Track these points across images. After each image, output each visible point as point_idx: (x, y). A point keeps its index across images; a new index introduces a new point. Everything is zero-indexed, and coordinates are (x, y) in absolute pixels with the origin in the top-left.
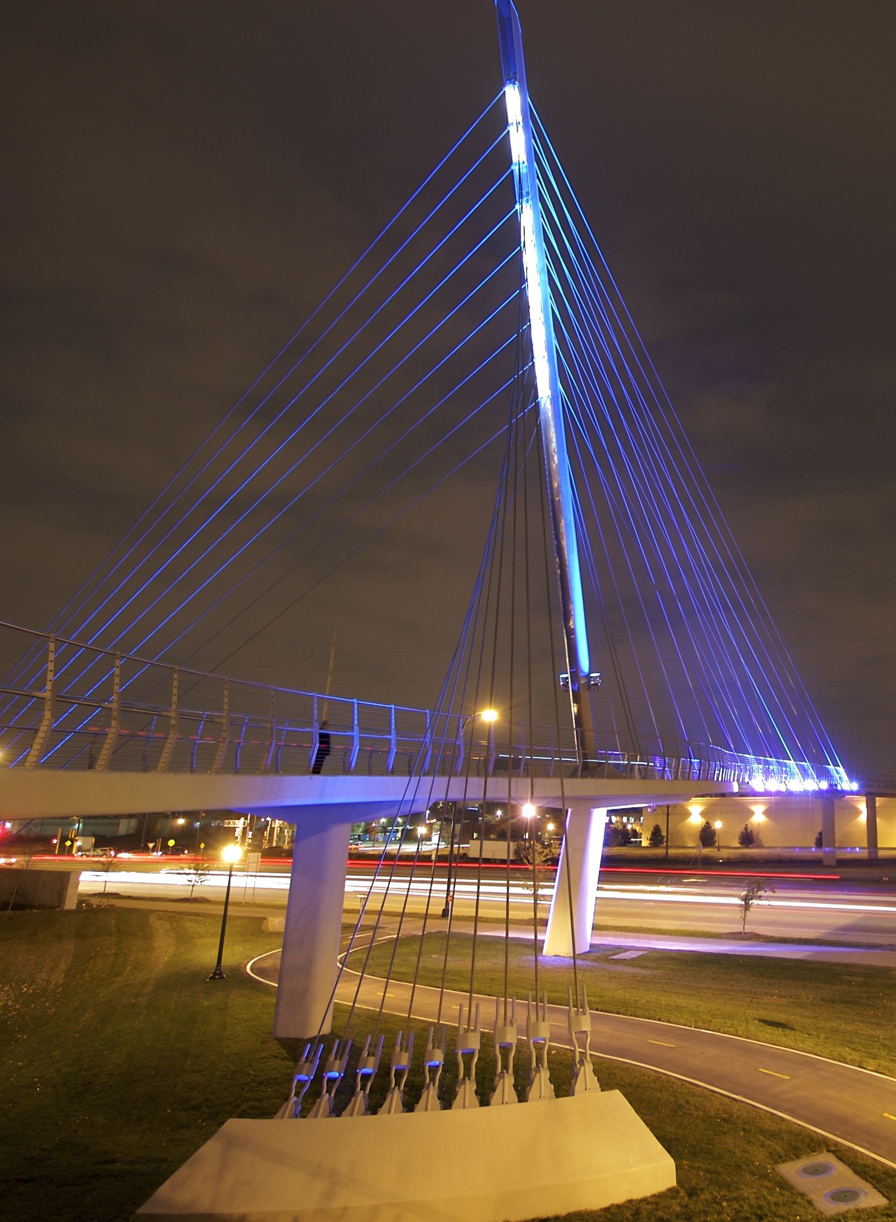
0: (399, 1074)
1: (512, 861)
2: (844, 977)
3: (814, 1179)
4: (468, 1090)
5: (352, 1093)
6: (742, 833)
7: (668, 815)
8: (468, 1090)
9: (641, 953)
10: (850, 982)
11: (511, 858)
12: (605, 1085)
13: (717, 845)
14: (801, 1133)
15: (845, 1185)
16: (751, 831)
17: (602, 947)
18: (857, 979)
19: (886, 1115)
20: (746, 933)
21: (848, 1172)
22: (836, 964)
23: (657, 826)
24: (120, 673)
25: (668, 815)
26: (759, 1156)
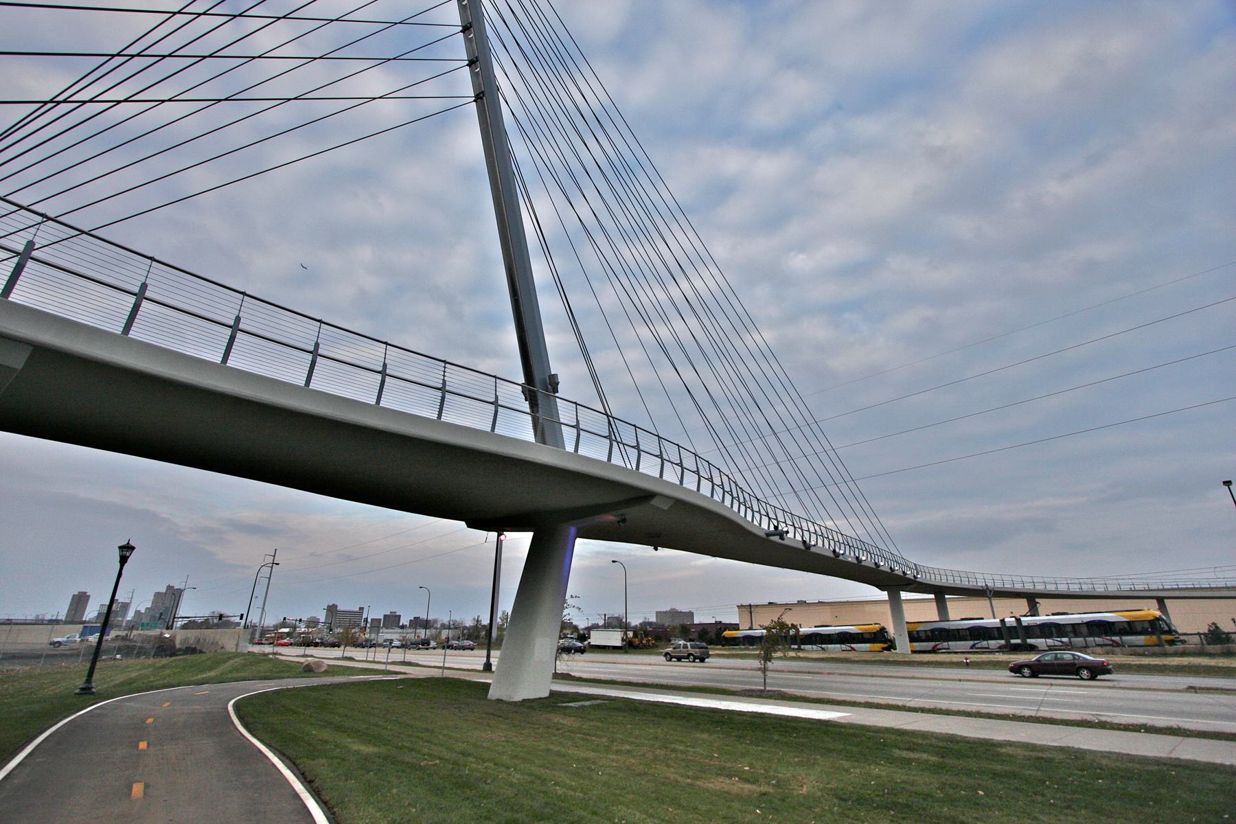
18: (925, 756)
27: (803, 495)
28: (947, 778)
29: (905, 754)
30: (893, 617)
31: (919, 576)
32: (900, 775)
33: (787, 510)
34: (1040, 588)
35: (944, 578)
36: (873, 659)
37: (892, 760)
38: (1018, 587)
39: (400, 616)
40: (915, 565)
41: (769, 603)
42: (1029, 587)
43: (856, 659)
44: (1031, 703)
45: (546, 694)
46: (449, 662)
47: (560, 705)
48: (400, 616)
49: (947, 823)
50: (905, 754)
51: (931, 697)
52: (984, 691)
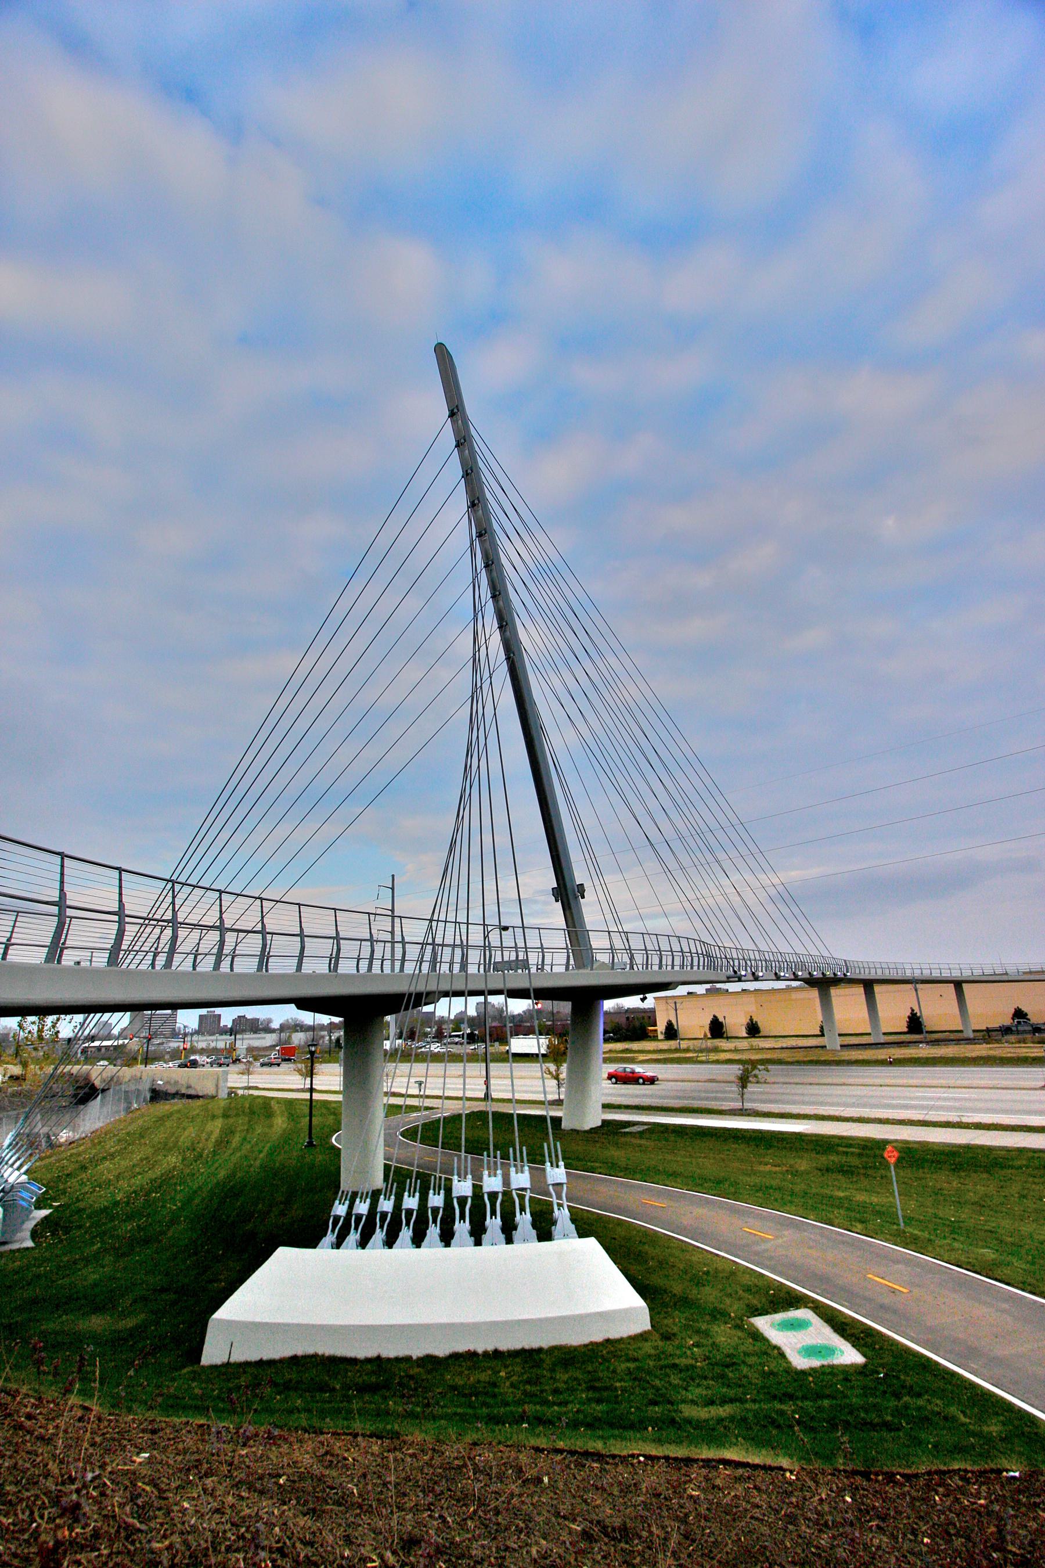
0: (383, 1220)
1: (543, 1055)
2: (841, 1149)
3: (790, 1334)
4: (406, 1234)
5: (373, 1232)
6: (748, 1024)
7: (676, 1010)
8: (406, 1234)
9: (646, 1127)
10: (846, 1153)
11: (543, 1051)
12: (582, 1234)
13: (725, 1036)
14: (790, 1291)
15: (820, 1341)
16: (756, 1022)
17: (780, 1136)
18: (854, 1150)
19: (870, 1276)
20: (746, 1110)
21: (827, 1331)
22: (833, 1137)
23: (670, 1021)
24: (557, 974)
25: (676, 1010)
26: (734, 1308)
27: (704, 828)
28: (864, 1159)
29: (845, 1149)
30: (822, 1010)
31: (848, 974)
32: (844, 1159)
33: (739, 947)
34: (967, 974)
35: (873, 971)
36: (805, 1059)
37: (838, 1153)
38: (946, 974)
39: (220, 1015)
40: (845, 961)
41: (688, 993)
42: (956, 974)
43: (789, 1060)
44: (923, 1107)
45: (599, 1124)
46: (433, 1089)
47: (623, 1130)
48: (220, 1015)
49: (936, 1567)
50: (845, 1149)
51: (858, 1106)
52: (899, 1098)
